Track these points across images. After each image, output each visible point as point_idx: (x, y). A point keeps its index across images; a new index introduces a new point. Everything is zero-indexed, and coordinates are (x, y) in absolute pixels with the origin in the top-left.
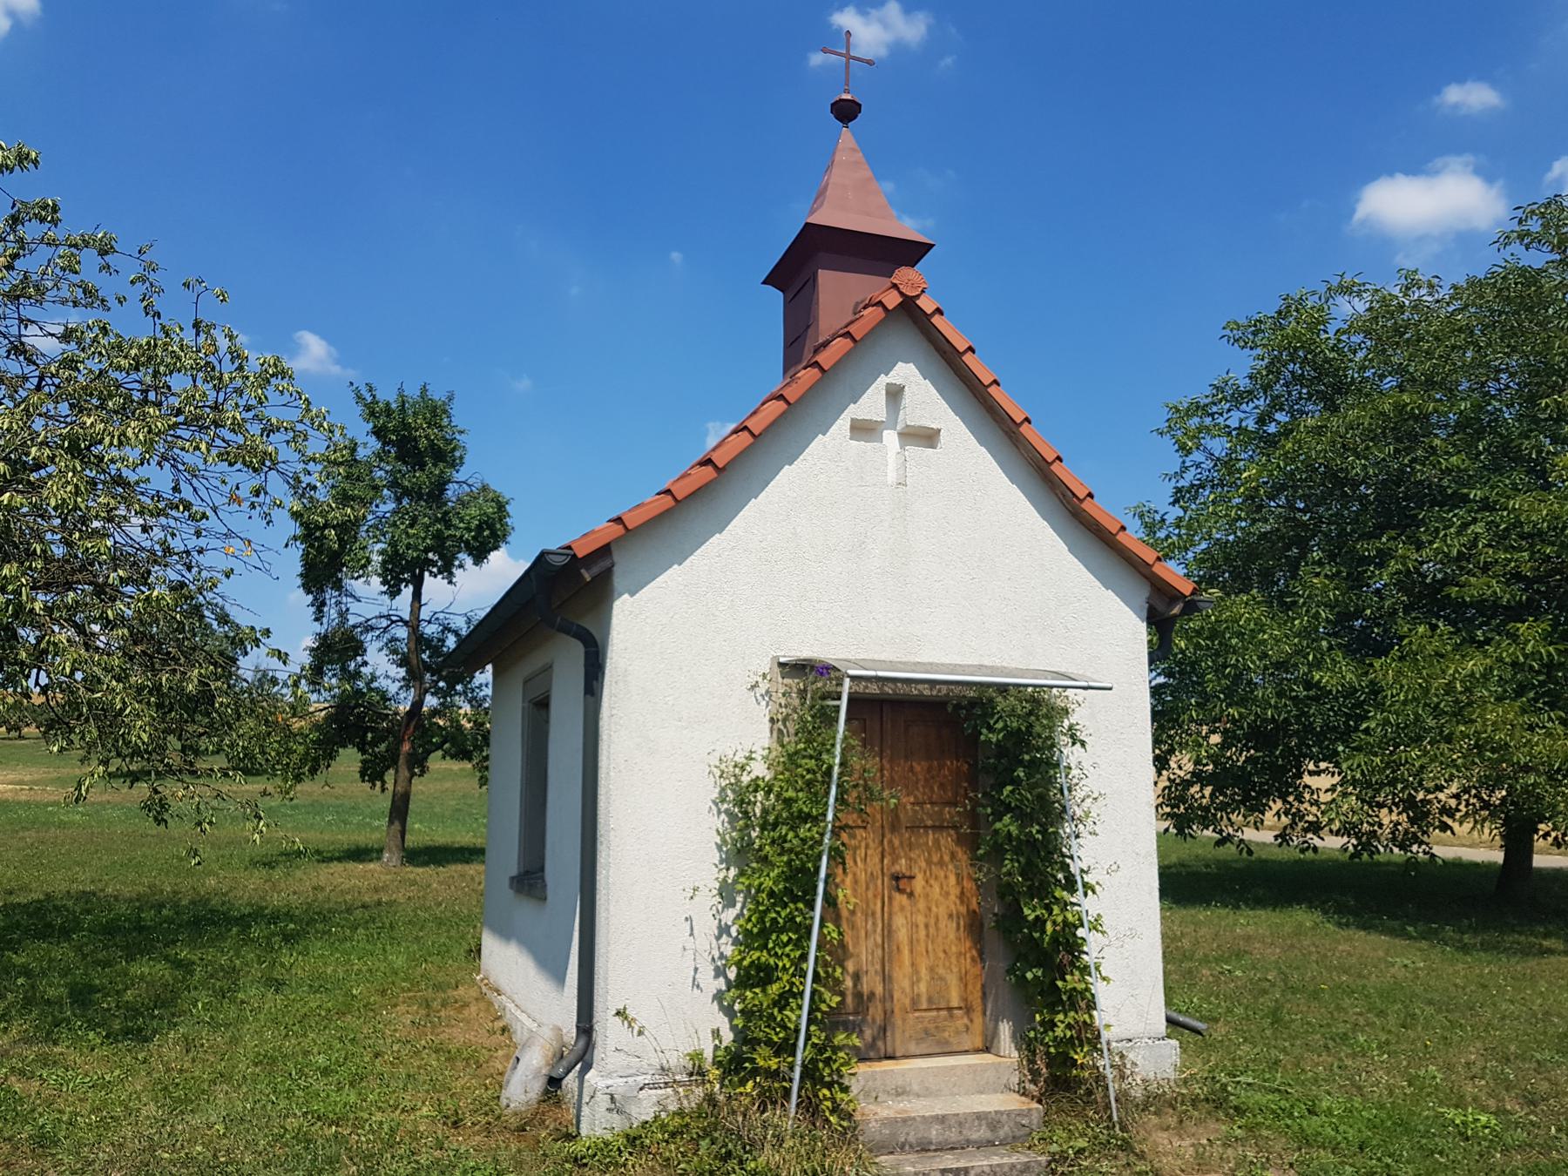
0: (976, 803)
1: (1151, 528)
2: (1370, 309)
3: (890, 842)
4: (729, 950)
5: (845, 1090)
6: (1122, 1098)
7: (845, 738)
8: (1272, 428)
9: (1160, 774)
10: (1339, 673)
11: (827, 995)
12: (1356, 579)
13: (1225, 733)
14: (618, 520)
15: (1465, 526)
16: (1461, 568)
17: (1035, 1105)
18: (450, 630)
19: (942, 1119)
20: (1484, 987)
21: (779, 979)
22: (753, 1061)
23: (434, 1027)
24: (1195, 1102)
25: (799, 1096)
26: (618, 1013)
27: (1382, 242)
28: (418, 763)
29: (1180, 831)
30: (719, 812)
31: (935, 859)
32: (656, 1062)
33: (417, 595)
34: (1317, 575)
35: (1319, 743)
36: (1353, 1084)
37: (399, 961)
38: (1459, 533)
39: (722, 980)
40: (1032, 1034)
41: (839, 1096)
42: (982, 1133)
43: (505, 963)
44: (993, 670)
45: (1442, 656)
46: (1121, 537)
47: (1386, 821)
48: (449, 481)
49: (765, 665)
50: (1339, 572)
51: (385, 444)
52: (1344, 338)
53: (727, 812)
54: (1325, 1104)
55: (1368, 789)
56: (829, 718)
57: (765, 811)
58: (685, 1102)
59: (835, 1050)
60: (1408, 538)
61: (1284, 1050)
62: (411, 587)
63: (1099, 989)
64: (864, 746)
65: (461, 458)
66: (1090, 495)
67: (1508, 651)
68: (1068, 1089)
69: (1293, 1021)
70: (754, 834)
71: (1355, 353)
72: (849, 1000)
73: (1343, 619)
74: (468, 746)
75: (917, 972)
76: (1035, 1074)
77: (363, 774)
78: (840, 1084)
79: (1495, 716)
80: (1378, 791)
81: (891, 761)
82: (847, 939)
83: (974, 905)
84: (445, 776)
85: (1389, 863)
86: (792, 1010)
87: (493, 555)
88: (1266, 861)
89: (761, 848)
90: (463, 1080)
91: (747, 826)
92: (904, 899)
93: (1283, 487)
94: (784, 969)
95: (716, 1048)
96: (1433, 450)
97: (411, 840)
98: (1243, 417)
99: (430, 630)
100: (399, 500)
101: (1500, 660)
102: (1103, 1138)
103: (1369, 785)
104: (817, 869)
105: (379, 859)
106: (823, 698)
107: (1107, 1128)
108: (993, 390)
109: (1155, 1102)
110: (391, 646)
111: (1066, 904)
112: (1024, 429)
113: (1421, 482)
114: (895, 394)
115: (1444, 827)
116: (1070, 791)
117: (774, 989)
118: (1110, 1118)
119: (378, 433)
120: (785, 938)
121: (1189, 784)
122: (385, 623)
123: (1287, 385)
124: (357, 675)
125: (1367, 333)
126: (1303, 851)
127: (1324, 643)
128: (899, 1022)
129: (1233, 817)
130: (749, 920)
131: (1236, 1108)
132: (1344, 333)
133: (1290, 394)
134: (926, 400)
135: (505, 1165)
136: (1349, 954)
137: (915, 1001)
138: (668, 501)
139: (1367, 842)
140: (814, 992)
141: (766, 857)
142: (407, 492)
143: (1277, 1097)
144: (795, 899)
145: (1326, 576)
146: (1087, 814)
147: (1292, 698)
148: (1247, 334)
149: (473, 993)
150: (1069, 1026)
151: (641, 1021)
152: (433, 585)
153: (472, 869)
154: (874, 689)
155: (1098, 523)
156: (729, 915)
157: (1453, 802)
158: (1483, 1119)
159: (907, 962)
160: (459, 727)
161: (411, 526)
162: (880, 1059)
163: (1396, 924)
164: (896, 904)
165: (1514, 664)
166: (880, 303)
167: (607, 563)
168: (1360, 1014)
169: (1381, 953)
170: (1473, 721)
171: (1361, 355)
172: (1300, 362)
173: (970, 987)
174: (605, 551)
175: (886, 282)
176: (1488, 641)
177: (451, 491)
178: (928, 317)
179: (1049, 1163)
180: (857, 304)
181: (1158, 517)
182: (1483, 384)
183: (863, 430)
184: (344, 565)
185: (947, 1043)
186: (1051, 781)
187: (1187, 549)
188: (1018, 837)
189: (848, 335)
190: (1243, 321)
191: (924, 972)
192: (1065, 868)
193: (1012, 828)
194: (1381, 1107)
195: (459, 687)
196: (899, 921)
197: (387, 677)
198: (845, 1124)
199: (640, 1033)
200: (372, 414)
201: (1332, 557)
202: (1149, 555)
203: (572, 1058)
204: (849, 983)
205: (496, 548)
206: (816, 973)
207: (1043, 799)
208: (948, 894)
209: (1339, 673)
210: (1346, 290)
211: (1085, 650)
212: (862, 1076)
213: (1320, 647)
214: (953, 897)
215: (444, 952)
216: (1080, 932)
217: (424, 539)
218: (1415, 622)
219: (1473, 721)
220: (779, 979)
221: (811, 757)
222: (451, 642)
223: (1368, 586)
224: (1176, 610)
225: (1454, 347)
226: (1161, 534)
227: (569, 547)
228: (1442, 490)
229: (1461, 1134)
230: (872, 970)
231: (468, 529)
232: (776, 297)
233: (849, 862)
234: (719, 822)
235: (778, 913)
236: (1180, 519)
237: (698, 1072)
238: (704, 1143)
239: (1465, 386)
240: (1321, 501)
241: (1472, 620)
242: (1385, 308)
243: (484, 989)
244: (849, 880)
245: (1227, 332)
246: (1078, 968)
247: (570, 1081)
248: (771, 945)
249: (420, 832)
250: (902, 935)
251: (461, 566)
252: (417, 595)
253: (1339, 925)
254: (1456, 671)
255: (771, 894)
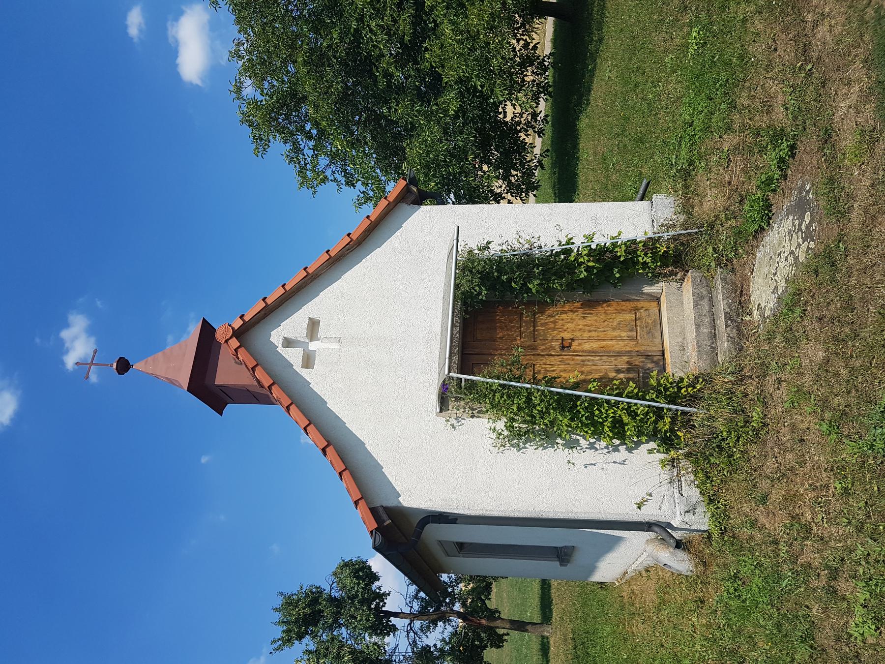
0: (521, 303)
1: (367, 199)
2: (250, 77)
3: (542, 351)
4: (603, 444)
5: (682, 380)
6: (685, 225)
7: (484, 376)
8: (314, 132)
9: (504, 198)
10: (451, 100)
11: (629, 389)
12: (399, 89)
13: (481, 162)
14: (356, 503)
15: (371, 31)
16: (395, 34)
17: (689, 274)
18: (417, 595)
19: (698, 326)
20: (622, 30)
21: (620, 416)
22: (666, 432)
23: (646, 611)
24: (686, 187)
25: (686, 406)
26: (639, 508)
27: (213, 72)
28: (493, 615)
29: (536, 188)
30: (525, 448)
31: (552, 326)
32: (667, 486)
33: (396, 615)
34: (396, 110)
35: (488, 112)
36: (675, 102)
37: (608, 629)
38: (375, 34)
39: (620, 448)
40: (650, 275)
41: (685, 383)
42: (705, 303)
43: (609, 569)
44: (446, 292)
45: (442, 45)
46: (373, 219)
47: (532, 78)
48: (330, 595)
49: (441, 420)
50: (395, 98)
51: (307, 633)
52: (265, 91)
53: (525, 443)
54: (687, 117)
55: (513, 87)
56: (472, 385)
57: (525, 422)
58: (689, 470)
59: (659, 385)
60: (377, 61)
61: (657, 137)
62: (391, 618)
63: (625, 237)
64: (487, 365)
65: (317, 588)
66: (349, 235)
67: (440, 11)
68: (680, 256)
69: (641, 132)
70: (537, 428)
71: (274, 86)
72: (631, 376)
73: (421, 97)
74: (483, 586)
75: (615, 337)
76: (672, 273)
77: (499, 647)
78: (679, 382)
79: (475, 20)
80: (515, 82)
81: (496, 350)
82: (597, 376)
83: (578, 305)
84: (500, 599)
85: (554, 77)
86: (638, 409)
87: (374, 570)
88: (552, 141)
89: (546, 425)
90: (676, 596)
91: (533, 432)
92: (575, 344)
93: (347, 127)
94: (614, 413)
95: (658, 451)
96: (329, 47)
97: (537, 619)
98: (307, 147)
99: (416, 606)
100: (340, 626)
101: (445, 15)
102: (707, 238)
103: (512, 86)
104: (558, 393)
105: (547, 638)
106: (460, 388)
107: (701, 235)
108: (288, 288)
109: (686, 208)
110: (425, 630)
111: (578, 254)
112: (310, 271)
113: (347, 53)
114: (288, 343)
115: (535, 47)
116: (514, 251)
117: (626, 419)
118: (696, 233)
119: (300, 637)
120: (597, 412)
121: (510, 182)
122: (412, 634)
123: (290, 123)
124: (441, 650)
125: (264, 79)
126: (547, 123)
127: (434, 108)
128: (643, 348)
129: (528, 159)
130: (586, 432)
131: (690, 165)
132: (262, 91)
133: (296, 122)
134: (292, 325)
135: (725, 575)
136: (604, 100)
137: (631, 339)
138: (346, 474)
139: (542, 88)
140: (627, 397)
141: (550, 422)
142: (336, 621)
143: (683, 143)
144: (575, 406)
145: (397, 105)
146: (528, 241)
147: (463, 126)
148: (261, 144)
149: (625, 587)
150: (646, 254)
151: (644, 494)
152: (390, 605)
153: (554, 584)
154: (455, 358)
155: (365, 231)
156: (583, 442)
157: (522, 42)
158: (694, 34)
159: (610, 343)
160: (473, 590)
161: (355, 618)
162: (664, 359)
163: (587, 75)
164: (577, 348)
165: (447, 8)
166: (236, 350)
167: (381, 510)
168: (637, 96)
169: (603, 83)
170: (478, 31)
171: (275, 83)
172: (278, 116)
173: (624, 308)
174: (374, 511)
175: (224, 346)
176: (435, 21)
177: (336, 594)
178: (245, 323)
179: (721, 267)
180: (236, 362)
181: (362, 195)
182: (294, 18)
183: (308, 361)
184: (377, 658)
185: (654, 321)
186: (509, 261)
187: (380, 180)
188: (541, 280)
189: (253, 369)
190: (254, 146)
191: (616, 333)
192: (558, 254)
193: (536, 283)
194: (688, 87)
195: (450, 590)
196: (587, 346)
197: (443, 632)
198: (701, 380)
199: (650, 495)
200: (289, 641)
201: (386, 102)
202: (383, 203)
203: (664, 535)
204: (622, 376)
205: (370, 568)
206: (616, 395)
207: (520, 266)
208: (572, 319)
209: (451, 100)
210: (239, 90)
211: (435, 240)
212: (674, 370)
213: (437, 110)
214: (574, 316)
215: (602, 603)
216: (594, 246)
217: (363, 611)
218: (423, 59)
219: (478, 31)
220: (620, 416)
221: (494, 395)
222: (422, 594)
223: (403, 83)
224: (415, 189)
225: (273, 33)
226: (371, 194)
227: (371, 532)
228: (351, 42)
229: (703, 46)
230: (614, 363)
231: (359, 584)
232: (230, 408)
233: (554, 374)
234: (530, 449)
235: (583, 416)
236: (363, 183)
237: (672, 463)
238: (712, 460)
239: (294, 28)
240: (355, 106)
241: (423, 29)
242: (250, 69)
243: (624, 581)
244: (564, 375)
245: (260, 155)
246: (613, 249)
247: (677, 535)
248: (601, 420)
249: (532, 614)
250: (595, 345)
251: (380, 588)
252: (396, 615)
253: (588, 104)
254: (450, 38)
255: (572, 419)
